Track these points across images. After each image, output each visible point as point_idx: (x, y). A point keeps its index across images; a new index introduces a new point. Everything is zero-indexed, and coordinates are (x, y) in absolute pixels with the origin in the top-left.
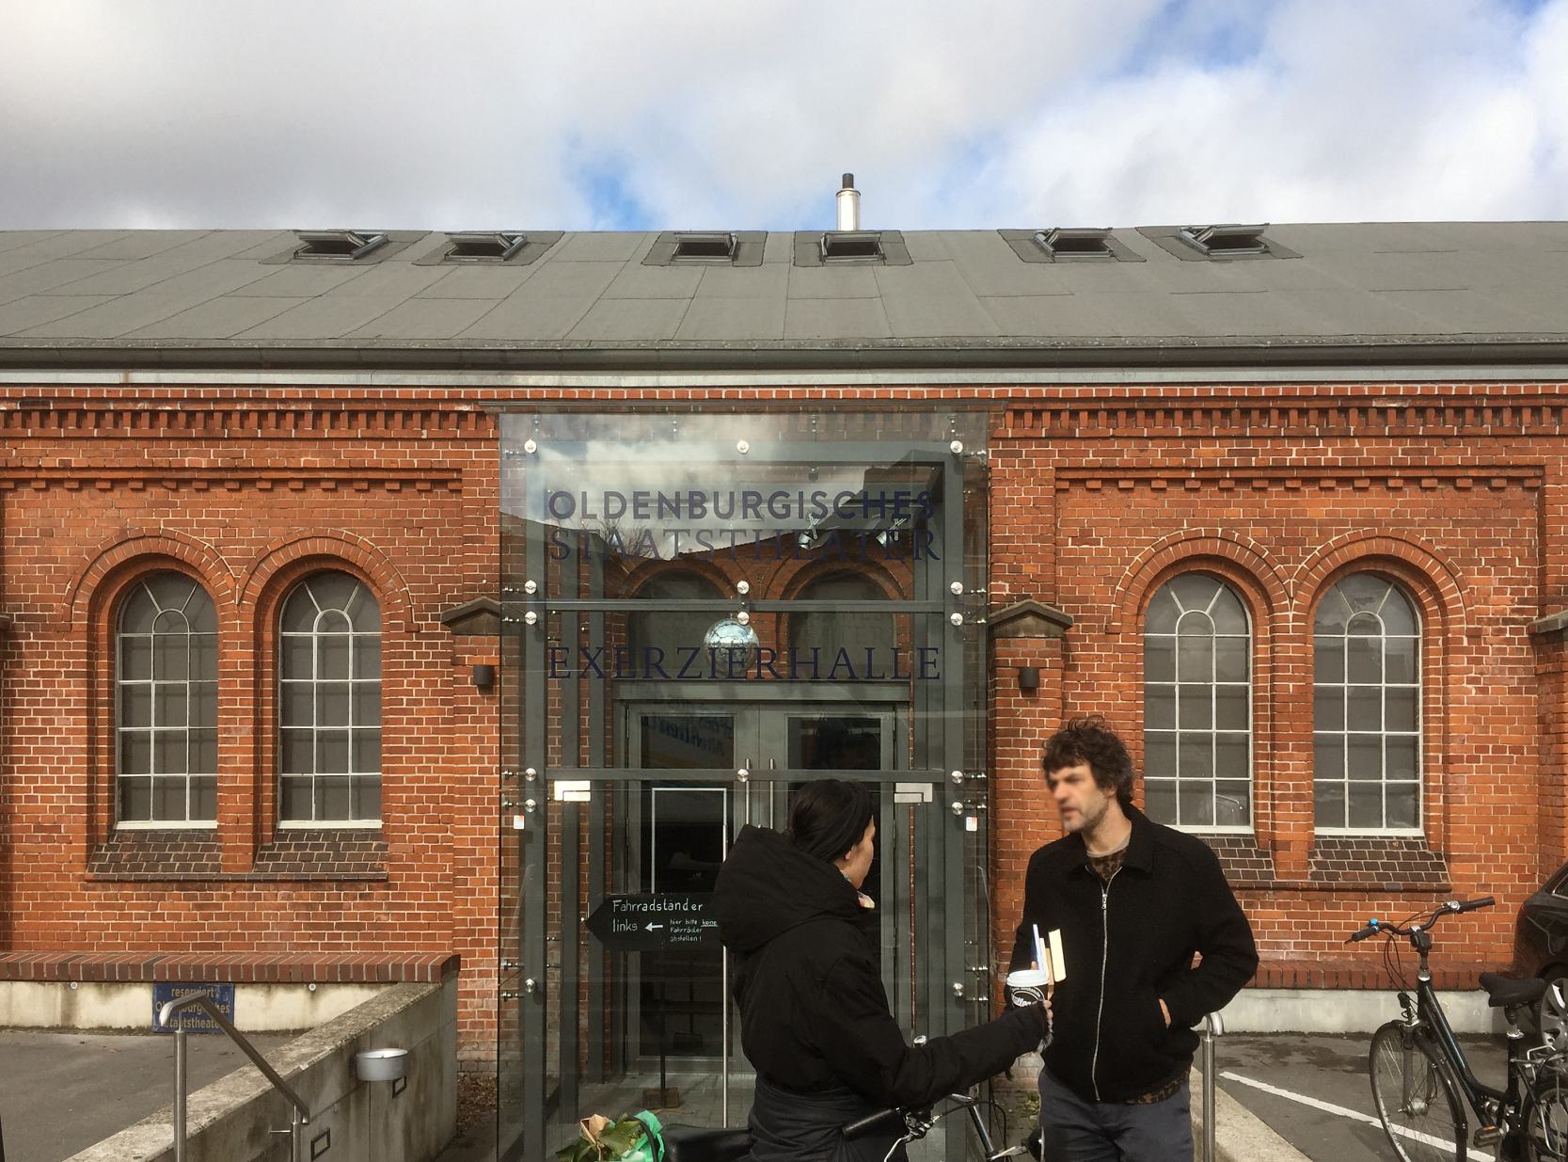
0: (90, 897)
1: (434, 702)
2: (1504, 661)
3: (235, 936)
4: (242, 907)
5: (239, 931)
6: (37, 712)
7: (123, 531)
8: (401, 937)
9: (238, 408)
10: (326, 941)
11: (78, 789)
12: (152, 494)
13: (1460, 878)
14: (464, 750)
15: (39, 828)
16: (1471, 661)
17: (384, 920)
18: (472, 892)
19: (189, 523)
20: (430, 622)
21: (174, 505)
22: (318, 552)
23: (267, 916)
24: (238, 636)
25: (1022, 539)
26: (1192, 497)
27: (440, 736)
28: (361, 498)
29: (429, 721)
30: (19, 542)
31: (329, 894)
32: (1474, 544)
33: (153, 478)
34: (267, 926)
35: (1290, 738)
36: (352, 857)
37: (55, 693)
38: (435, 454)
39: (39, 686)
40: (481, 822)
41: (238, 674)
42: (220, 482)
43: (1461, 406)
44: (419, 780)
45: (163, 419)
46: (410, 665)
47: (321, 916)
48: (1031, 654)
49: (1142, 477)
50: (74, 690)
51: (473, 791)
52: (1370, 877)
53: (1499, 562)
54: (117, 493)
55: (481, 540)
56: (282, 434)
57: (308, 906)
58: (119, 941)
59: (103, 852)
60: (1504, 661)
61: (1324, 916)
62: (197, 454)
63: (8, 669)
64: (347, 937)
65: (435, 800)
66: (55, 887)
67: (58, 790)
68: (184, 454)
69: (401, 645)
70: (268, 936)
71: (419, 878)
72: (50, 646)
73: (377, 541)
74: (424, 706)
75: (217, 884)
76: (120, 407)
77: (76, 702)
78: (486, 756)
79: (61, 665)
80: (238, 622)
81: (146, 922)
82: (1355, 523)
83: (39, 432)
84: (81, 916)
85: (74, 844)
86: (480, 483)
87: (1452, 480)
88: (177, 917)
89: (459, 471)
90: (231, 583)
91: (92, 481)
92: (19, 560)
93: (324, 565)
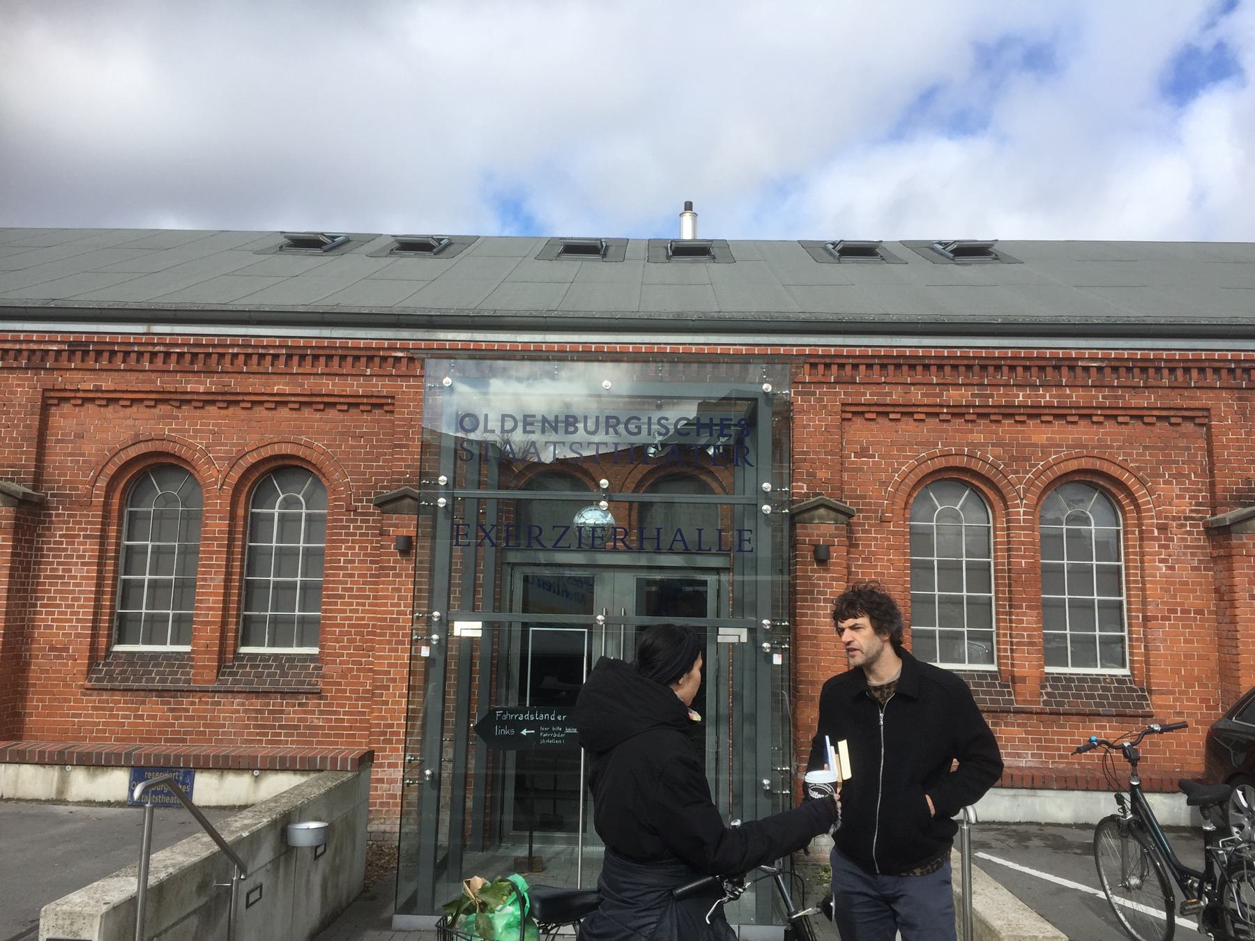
1: (364, 562)
2: (1186, 547)
4: (205, 711)
6: (59, 563)
7: (137, 435)
8: (328, 736)
9: (231, 351)
13: (1160, 707)
15: (52, 649)
16: (1160, 546)
17: (316, 723)
18: (386, 703)
22: (283, 452)
23: (225, 718)
24: (218, 511)
25: (817, 453)
26: (945, 426)
28: (318, 415)
30: (58, 441)
31: (274, 703)
32: (1159, 462)
33: (162, 398)
34: (223, 726)
35: (1024, 600)
37: (74, 550)
38: (376, 386)
40: (396, 650)
41: (216, 539)
42: (213, 402)
43: (1145, 366)
44: (350, 618)
45: (174, 358)
46: (347, 534)
47: (268, 719)
48: (824, 535)
49: (907, 411)
51: (391, 628)
52: (1089, 705)
53: (1179, 476)
54: (135, 409)
56: (261, 369)
57: (257, 711)
59: (100, 667)
60: (1186, 547)
61: (1054, 733)
62: (197, 382)
65: (361, 634)
66: (61, 693)
67: (71, 621)
68: (187, 382)
69: (341, 520)
70: (224, 733)
71: (345, 691)
72: (74, 516)
73: (328, 446)
75: (187, 694)
76: (142, 349)
78: (402, 602)
79: (81, 529)
82: (1068, 447)
83: (80, 365)
84: (79, 716)
87: (1141, 417)
88: (154, 717)
89: (393, 398)
90: (215, 473)
92: (57, 454)
93: (287, 462)
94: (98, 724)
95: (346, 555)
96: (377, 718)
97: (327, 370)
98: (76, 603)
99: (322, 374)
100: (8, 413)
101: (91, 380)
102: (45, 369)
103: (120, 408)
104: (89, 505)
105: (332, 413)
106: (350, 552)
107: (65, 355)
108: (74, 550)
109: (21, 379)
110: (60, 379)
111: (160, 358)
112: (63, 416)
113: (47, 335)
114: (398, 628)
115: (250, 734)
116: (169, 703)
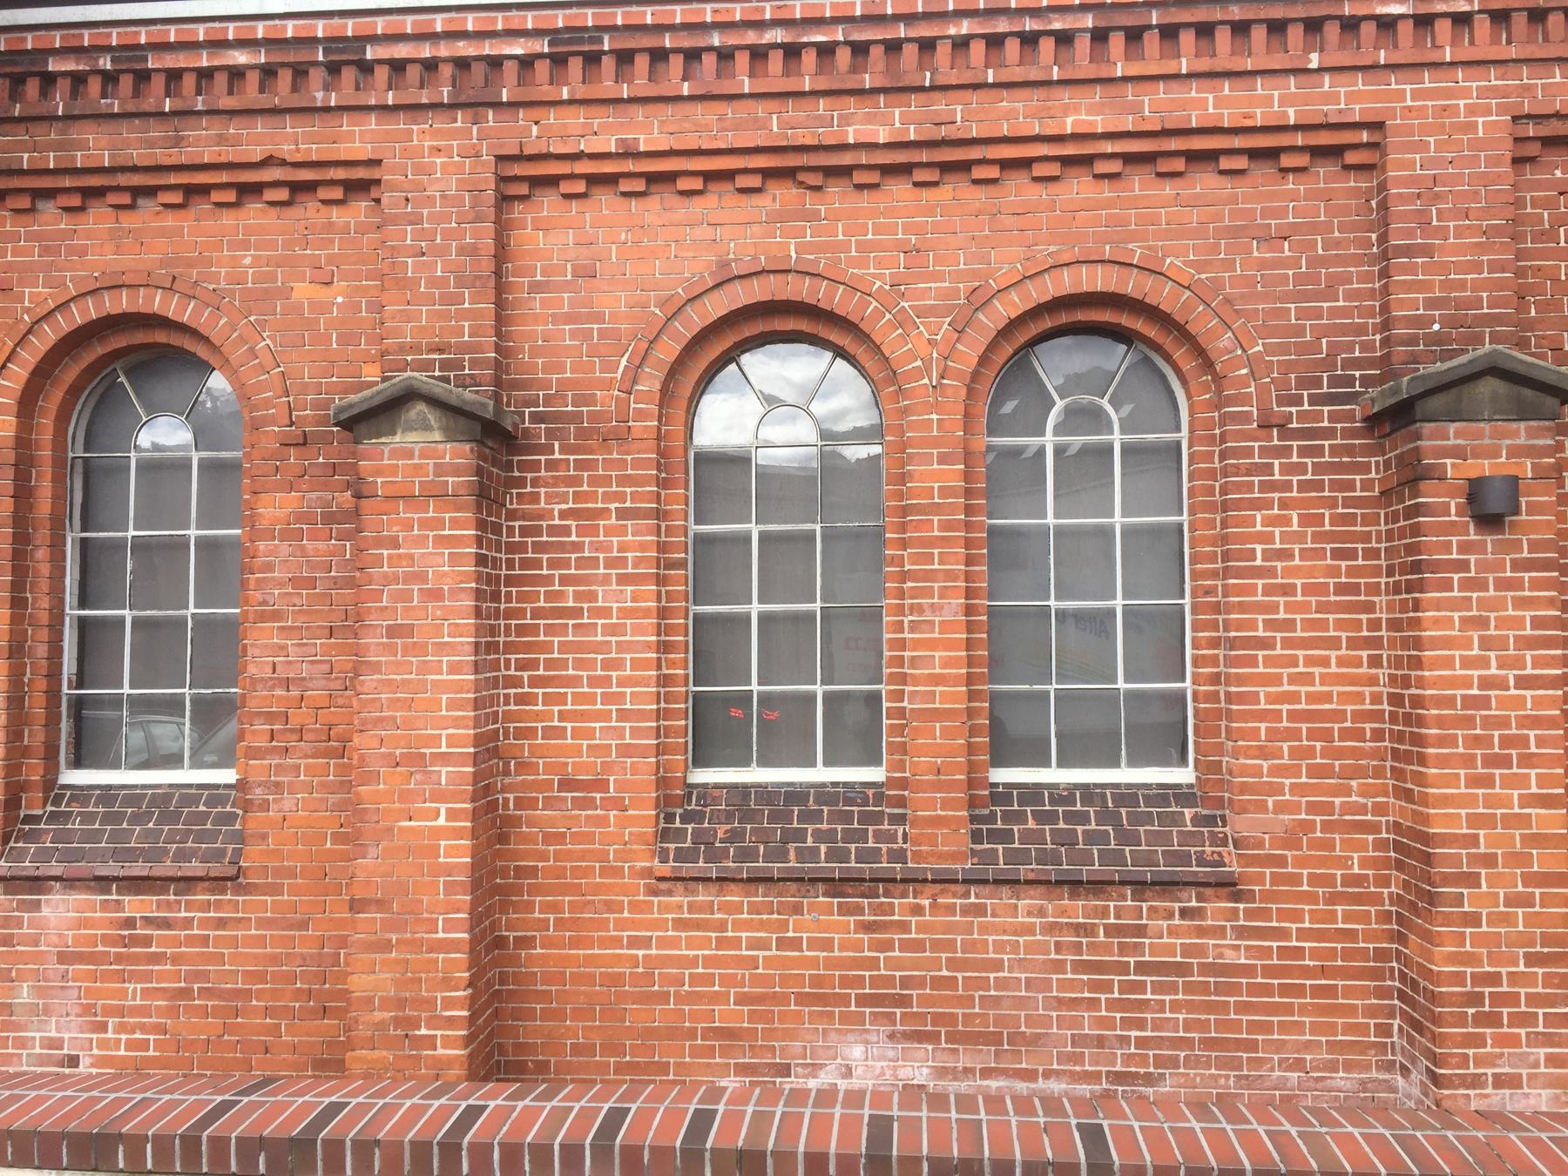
0: (663, 908)
1: (1318, 554)
3: (938, 982)
4: (950, 928)
5: (945, 973)
6: (564, 580)
7: (724, 265)
8: (1266, 990)
9: (952, 31)
10: (1116, 995)
11: (641, 715)
12: (774, 199)
14: (1447, 643)
15: (566, 785)
17: (1230, 958)
18: (1473, 919)
19: (845, 247)
20: (1306, 407)
21: (813, 216)
22: (1085, 288)
23: (1000, 947)
24: (935, 442)
27: (1331, 617)
28: (1168, 189)
29: (1309, 590)
30: (536, 287)
31: (1119, 907)
34: (997, 965)
36: (1155, 838)
37: (597, 547)
38: (1332, 98)
39: (569, 535)
40: (1488, 781)
41: (936, 509)
44: (1293, 697)
46: (1267, 487)
47: (1107, 948)
50: (635, 542)
51: (1469, 722)
54: (710, 200)
55: (1426, 251)
56: (1034, 74)
57: (1078, 929)
58: (717, 988)
59: (678, 824)
62: (870, 119)
63: (515, 506)
64: (1158, 988)
65: (1326, 735)
66: (599, 889)
67: (604, 716)
68: (845, 121)
69: (1248, 452)
70: (1001, 984)
71: (1295, 879)
74: (1297, 562)
75: (901, 886)
76: (733, 39)
77: (638, 562)
78: (1492, 654)
79: (607, 497)
80: (934, 417)
81: (767, 953)
83: (582, 92)
84: (645, 943)
85: (631, 812)
86: (1422, 146)
88: (827, 945)
90: (924, 349)
91: (670, 177)
92: (536, 319)
94: (693, 962)
95: (1268, 538)
96: (1453, 959)
97: (1204, 65)
98: (614, 674)
99: (1190, 76)
100: (416, 220)
101: (606, 128)
102: (497, 105)
103: (677, 197)
104: (622, 437)
105: (1204, 183)
106: (1277, 531)
107: (542, 68)
108: (597, 547)
109: (437, 134)
110: (535, 129)
111: (776, 61)
112: (540, 226)
113: (500, 15)
114: (1488, 722)
115: (1064, 985)
116: (859, 910)
